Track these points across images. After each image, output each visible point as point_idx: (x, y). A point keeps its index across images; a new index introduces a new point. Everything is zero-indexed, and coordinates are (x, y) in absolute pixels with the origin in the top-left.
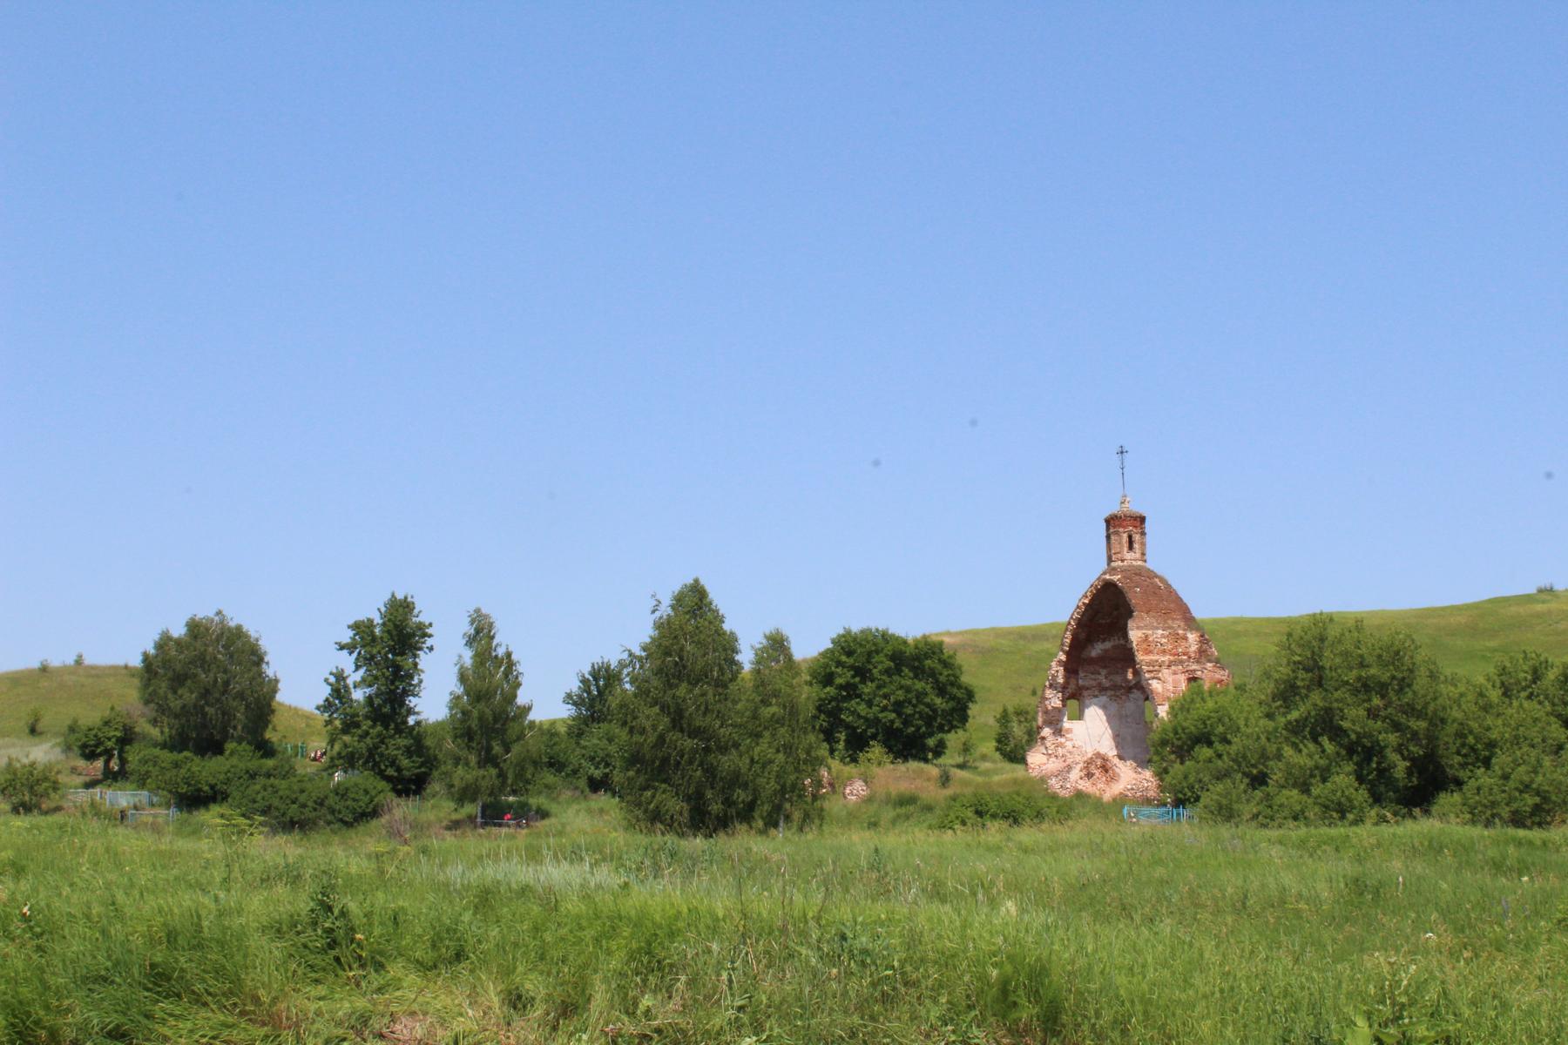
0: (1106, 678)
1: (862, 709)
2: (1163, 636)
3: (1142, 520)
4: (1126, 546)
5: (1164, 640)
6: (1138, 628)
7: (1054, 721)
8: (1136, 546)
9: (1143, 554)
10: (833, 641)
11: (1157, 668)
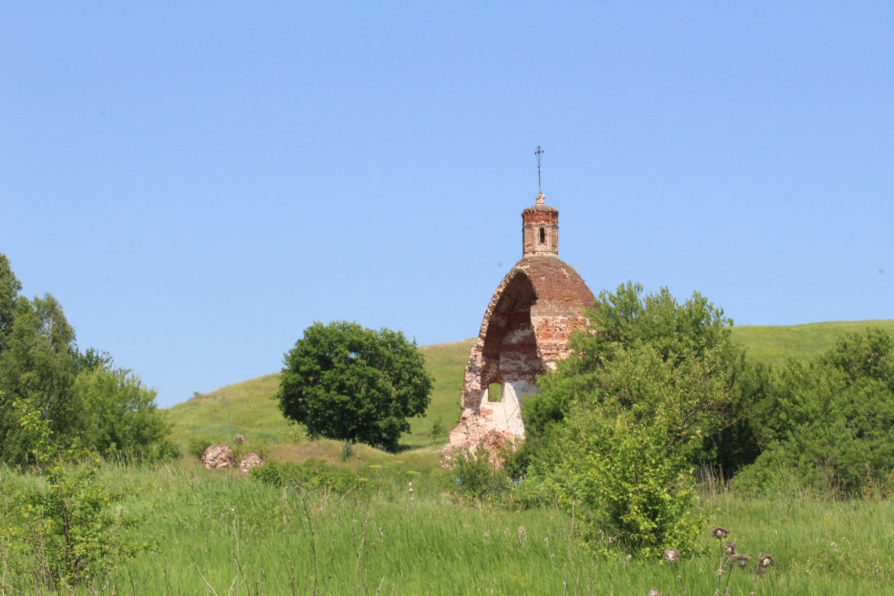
0: (525, 363)
1: (320, 392)
2: (562, 322)
3: (555, 214)
4: (537, 239)
5: (563, 325)
6: (540, 314)
7: (473, 402)
8: (547, 238)
9: (554, 246)
10: (306, 334)
11: (554, 351)
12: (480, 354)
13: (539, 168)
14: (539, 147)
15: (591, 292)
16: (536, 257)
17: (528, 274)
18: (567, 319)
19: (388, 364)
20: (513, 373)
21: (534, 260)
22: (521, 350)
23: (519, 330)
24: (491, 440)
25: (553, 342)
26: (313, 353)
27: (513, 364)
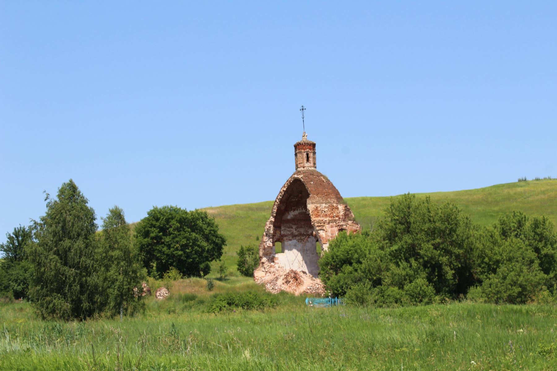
2: (325, 207)
3: (314, 145)
5: (326, 209)
6: (312, 203)
8: (311, 159)
11: (322, 224)
12: (272, 226)
13: (303, 118)
14: (303, 106)
15: (337, 190)
16: (306, 170)
17: (303, 180)
18: (328, 206)
19: (201, 230)
20: (289, 236)
21: (305, 172)
22: (293, 223)
23: (292, 211)
24: (292, 276)
25: (321, 219)
26: (157, 226)
27: (288, 231)
